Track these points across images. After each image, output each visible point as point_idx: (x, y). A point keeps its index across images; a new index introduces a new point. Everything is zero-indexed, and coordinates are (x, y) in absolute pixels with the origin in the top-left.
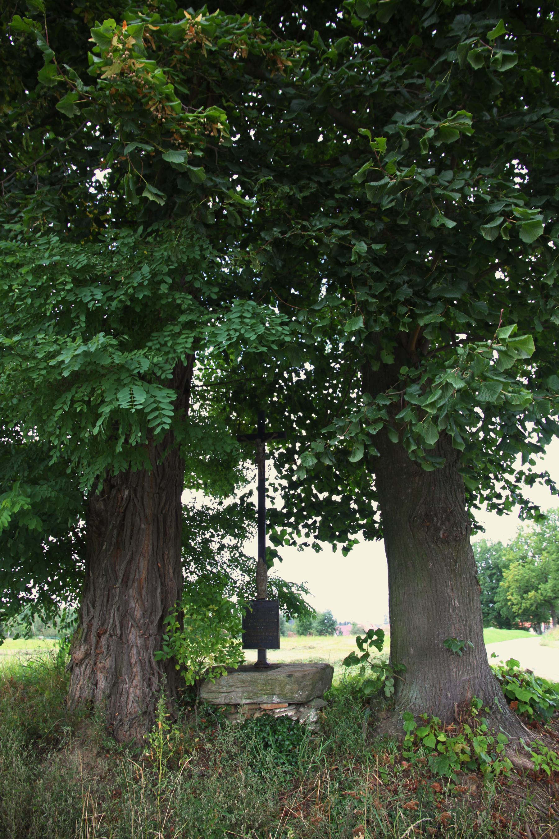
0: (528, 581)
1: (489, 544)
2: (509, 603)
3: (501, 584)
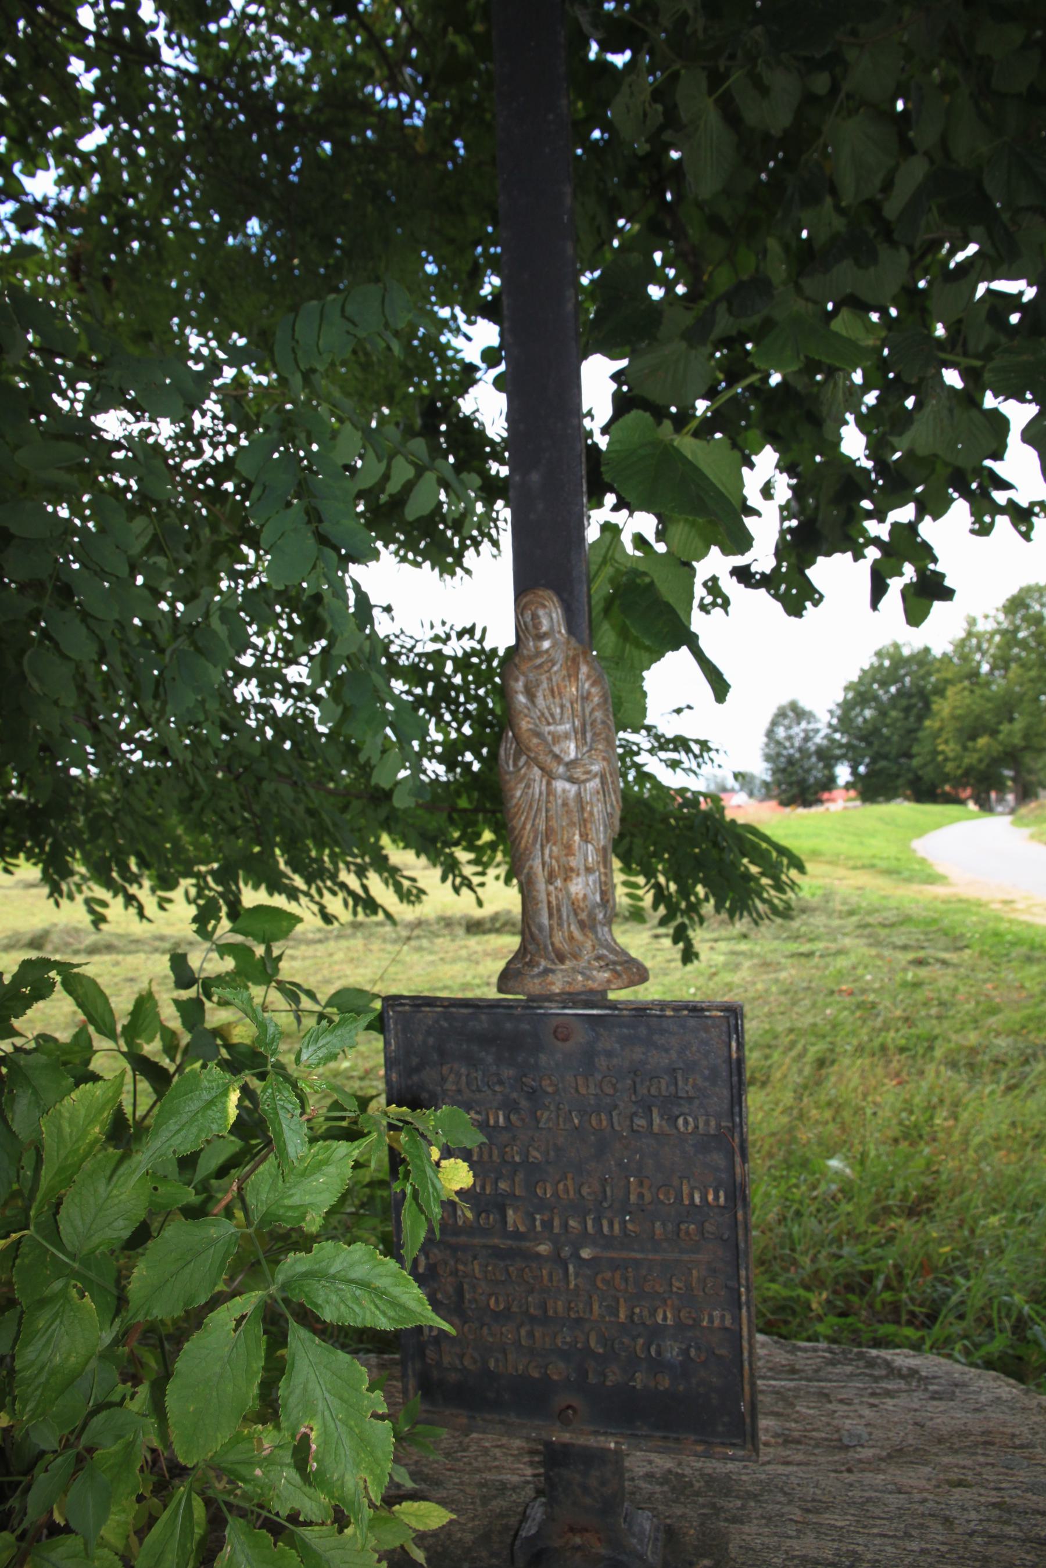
0: (978, 717)
1: (906, 652)
2: (940, 758)
3: (927, 723)
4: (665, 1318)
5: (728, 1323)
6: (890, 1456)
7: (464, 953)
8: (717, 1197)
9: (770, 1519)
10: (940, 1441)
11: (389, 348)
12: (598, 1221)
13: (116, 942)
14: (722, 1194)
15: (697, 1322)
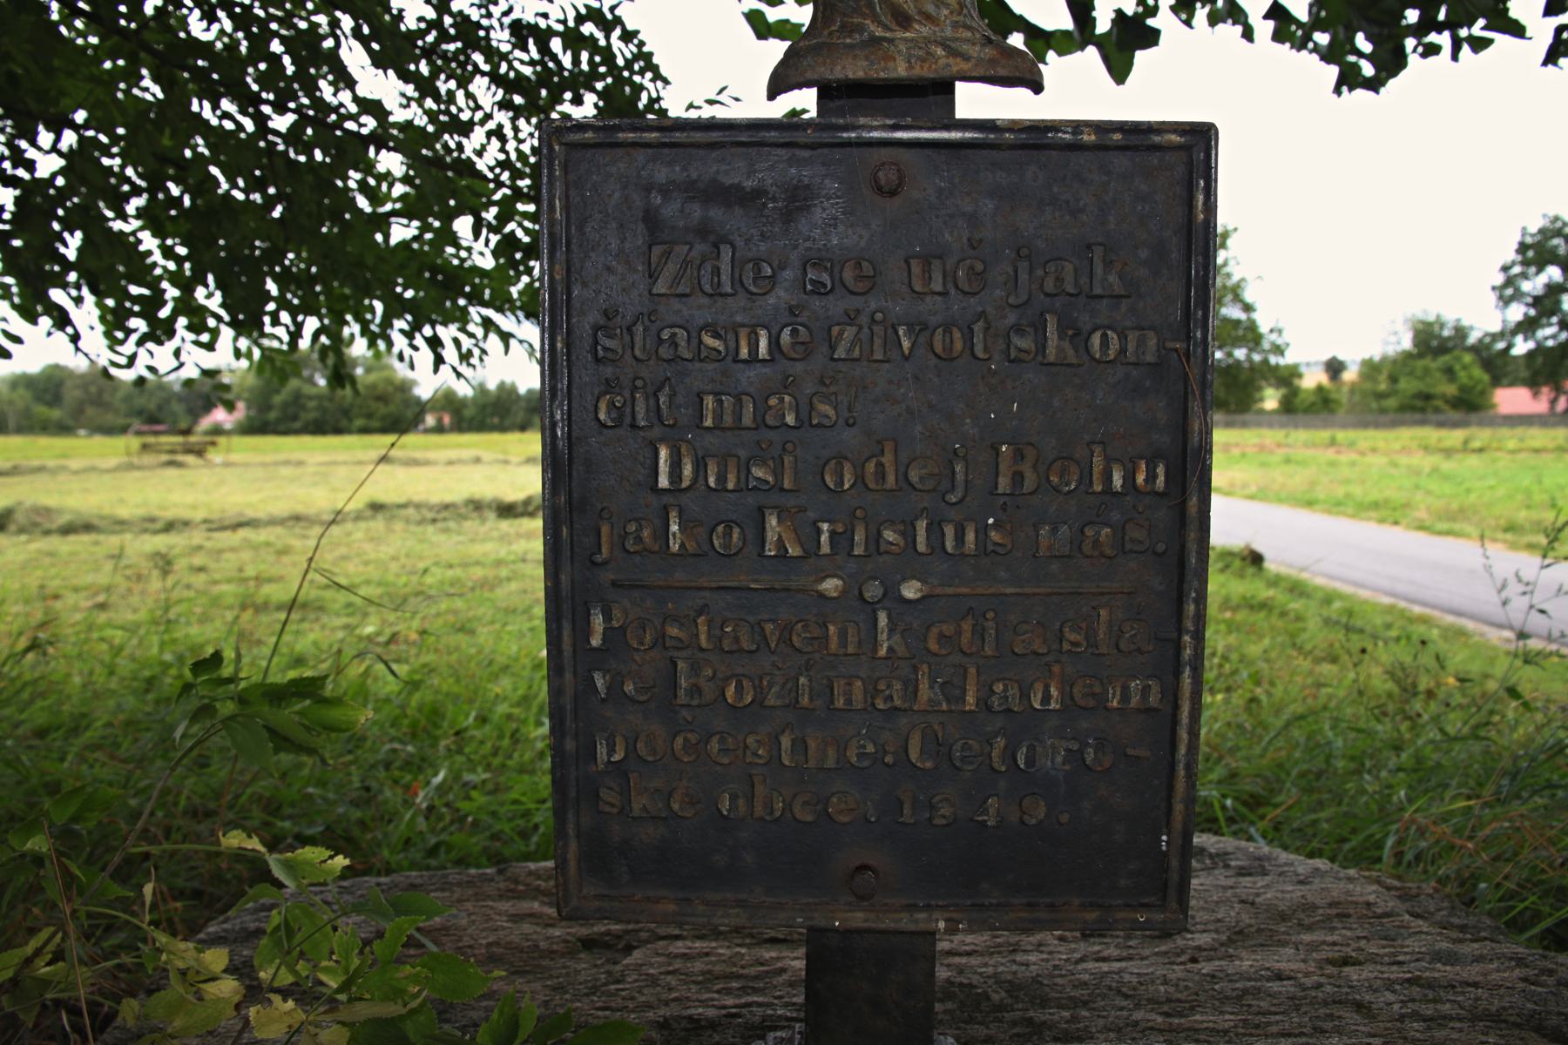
4: (1046, 698)
5: (1153, 700)
6: (1231, 941)
7: (495, 534)
8: (1151, 477)
9: (1119, 1030)
10: (1283, 917)
11: (323, 661)
12: (935, 529)
13: (96, 522)
14: (1161, 470)
15: (1102, 699)
